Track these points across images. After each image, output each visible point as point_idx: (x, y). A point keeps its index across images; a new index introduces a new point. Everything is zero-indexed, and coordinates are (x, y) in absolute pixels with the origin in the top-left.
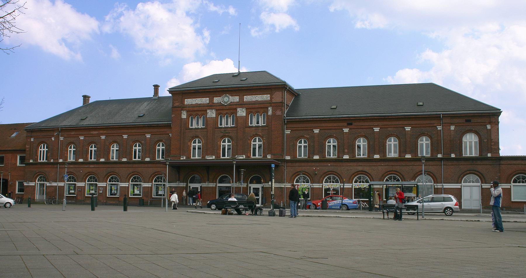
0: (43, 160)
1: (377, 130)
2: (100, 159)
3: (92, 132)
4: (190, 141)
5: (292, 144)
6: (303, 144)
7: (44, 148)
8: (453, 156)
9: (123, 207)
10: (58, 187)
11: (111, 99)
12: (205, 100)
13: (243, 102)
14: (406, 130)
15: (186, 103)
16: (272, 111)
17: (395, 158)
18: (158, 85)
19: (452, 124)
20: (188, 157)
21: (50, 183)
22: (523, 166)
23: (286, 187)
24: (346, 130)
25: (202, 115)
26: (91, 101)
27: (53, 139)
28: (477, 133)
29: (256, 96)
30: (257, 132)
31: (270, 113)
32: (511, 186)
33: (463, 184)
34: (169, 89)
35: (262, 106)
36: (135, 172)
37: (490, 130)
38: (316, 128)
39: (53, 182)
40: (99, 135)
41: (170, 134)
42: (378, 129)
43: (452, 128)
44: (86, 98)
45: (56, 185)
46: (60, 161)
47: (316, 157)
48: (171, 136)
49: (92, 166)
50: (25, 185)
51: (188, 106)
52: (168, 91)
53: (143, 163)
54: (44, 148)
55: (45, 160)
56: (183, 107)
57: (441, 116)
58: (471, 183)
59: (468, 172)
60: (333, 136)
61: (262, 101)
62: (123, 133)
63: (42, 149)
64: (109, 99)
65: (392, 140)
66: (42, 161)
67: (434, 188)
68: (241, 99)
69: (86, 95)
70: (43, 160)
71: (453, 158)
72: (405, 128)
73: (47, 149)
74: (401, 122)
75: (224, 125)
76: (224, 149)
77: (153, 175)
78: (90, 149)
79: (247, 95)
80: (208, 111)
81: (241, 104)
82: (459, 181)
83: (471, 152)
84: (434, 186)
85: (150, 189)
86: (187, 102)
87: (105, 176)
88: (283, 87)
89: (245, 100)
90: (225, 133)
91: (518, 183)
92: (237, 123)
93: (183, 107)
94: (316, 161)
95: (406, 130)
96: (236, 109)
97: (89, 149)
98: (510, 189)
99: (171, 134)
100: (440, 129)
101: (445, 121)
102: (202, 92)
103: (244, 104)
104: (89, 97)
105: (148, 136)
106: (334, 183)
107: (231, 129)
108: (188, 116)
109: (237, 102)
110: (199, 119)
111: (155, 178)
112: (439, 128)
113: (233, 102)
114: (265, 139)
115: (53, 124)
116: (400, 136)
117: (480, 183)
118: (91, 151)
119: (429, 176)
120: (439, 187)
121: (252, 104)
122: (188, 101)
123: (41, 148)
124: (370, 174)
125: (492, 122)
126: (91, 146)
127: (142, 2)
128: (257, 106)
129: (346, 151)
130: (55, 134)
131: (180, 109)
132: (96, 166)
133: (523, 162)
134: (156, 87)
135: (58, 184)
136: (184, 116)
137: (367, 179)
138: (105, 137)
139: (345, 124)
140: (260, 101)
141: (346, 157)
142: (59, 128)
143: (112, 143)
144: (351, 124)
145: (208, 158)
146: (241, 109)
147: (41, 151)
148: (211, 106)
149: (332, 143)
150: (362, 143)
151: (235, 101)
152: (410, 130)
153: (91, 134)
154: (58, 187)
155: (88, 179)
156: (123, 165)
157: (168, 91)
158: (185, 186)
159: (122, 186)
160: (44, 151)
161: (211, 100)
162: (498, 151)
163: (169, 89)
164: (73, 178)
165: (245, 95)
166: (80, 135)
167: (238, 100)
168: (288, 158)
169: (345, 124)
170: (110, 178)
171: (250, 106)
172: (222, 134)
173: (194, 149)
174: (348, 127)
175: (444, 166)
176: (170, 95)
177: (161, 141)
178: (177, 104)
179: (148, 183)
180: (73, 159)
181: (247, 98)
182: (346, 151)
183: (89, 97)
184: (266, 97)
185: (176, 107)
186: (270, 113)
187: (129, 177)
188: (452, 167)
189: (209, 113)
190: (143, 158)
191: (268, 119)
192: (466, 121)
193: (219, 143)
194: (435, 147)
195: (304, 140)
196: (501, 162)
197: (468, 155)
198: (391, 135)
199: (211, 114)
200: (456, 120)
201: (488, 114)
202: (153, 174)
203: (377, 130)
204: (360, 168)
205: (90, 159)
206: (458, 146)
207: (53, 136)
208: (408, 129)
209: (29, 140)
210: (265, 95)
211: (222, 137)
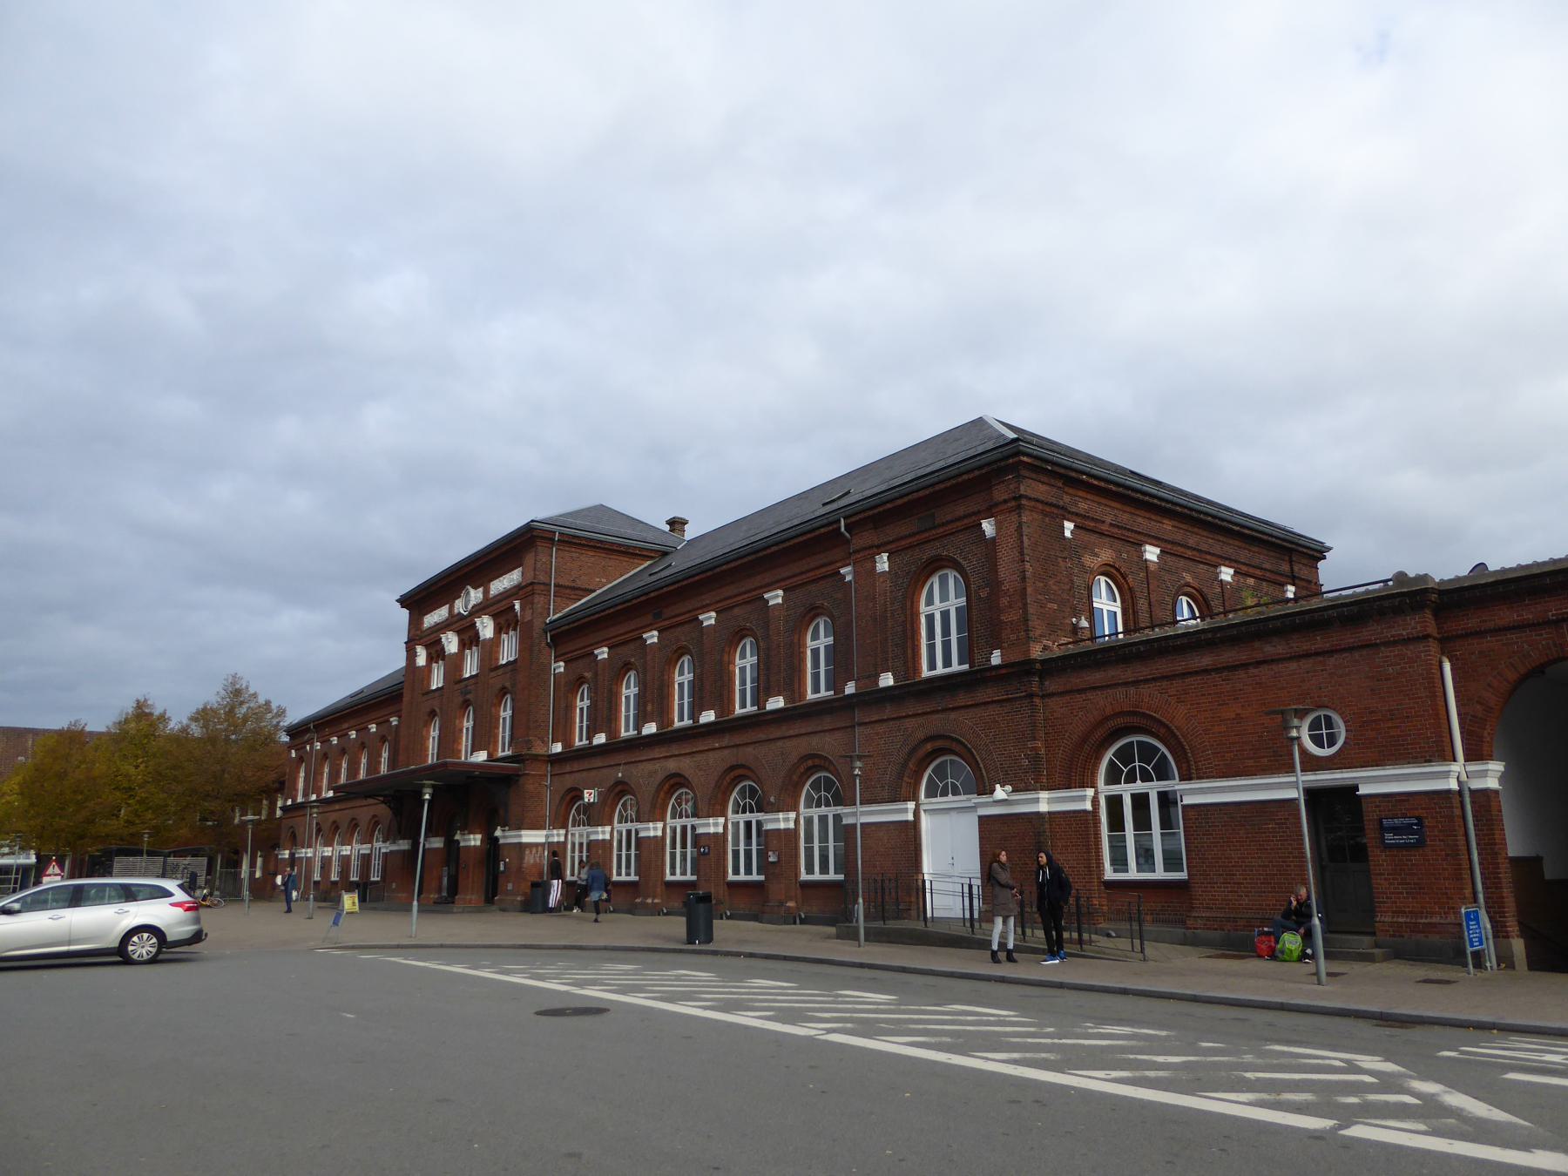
0: (947, 663)
7: (944, 598)
9: (684, 919)
10: (1468, 800)
17: (1523, 574)
22: (1132, 690)
23: (862, 824)
37: (993, 539)
48: (848, 578)
53: (762, 720)
54: (944, 598)
55: (956, 667)
58: (950, 797)
62: (641, 628)
63: (937, 607)
66: (940, 670)
70: (947, 663)
82: (902, 791)
97: (918, 614)
98: (915, 825)
106: (753, 812)
111: (819, 775)
123: (930, 602)
125: (996, 505)
127: (77, 731)
133: (1553, 608)
137: (1164, 756)
147: (930, 618)
154: (1468, 800)
155: (1111, 762)
160: (945, 615)
164: (1147, 752)
166: (596, 646)
170: (822, 774)
180: (960, 663)
188: (881, 728)
196: (1047, 683)
201: (753, 557)
204: (1103, 702)
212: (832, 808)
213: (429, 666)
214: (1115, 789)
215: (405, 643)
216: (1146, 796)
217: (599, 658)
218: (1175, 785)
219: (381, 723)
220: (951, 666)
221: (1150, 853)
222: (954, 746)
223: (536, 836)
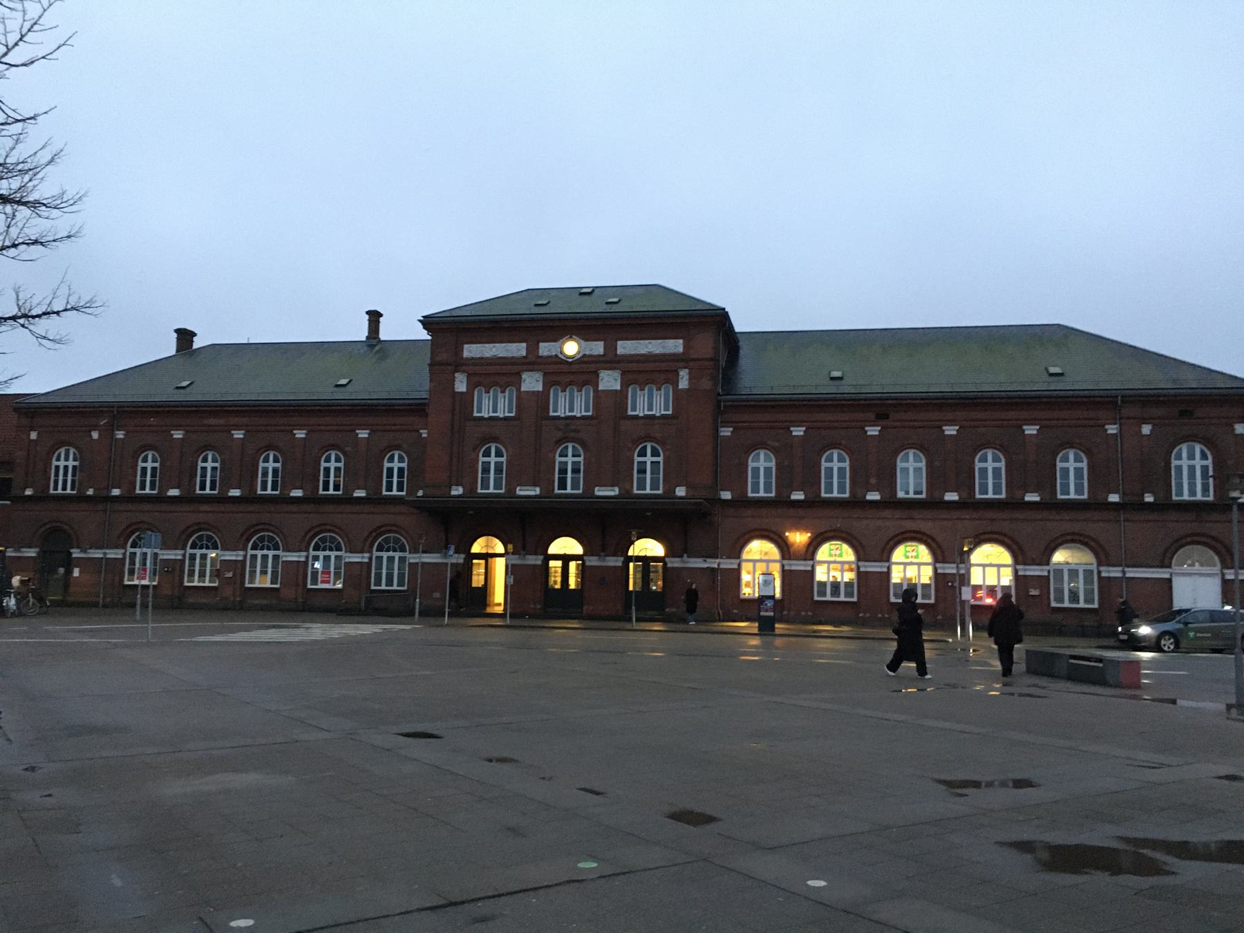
0: (64, 488)
1: (951, 430)
2: (228, 491)
3: (206, 422)
4: (476, 448)
5: (737, 461)
6: (836, 465)
8: (1149, 498)
11: (250, 342)
12: (517, 349)
13: (616, 355)
14: (1027, 432)
15: (466, 354)
16: (690, 379)
18: (379, 310)
19: (1145, 421)
20: (471, 490)
21: (522, 556)
24: (873, 431)
25: (507, 384)
26: (198, 343)
27: (95, 435)
28: (1207, 442)
29: (647, 341)
30: (650, 428)
31: (684, 384)
32: (1049, 572)
33: (1175, 569)
34: (422, 319)
35: (664, 366)
36: (325, 524)
38: (363, 426)
39: (90, 548)
40: (228, 430)
41: (421, 431)
42: (954, 430)
43: (1146, 429)
44: (185, 337)
45: (101, 556)
46: (113, 494)
47: (798, 496)
49: (205, 508)
50: (74, 556)
51: (473, 361)
52: (420, 321)
54: (67, 459)
56: (460, 364)
57: (1117, 401)
59: (1189, 539)
60: (984, 445)
61: (664, 355)
62: (357, 425)
64: (246, 342)
65: (911, 458)
66: (60, 491)
67: (1099, 577)
68: (533, 349)
69: (185, 329)
70: (64, 488)
71: (1149, 503)
72: (792, 429)
73: (76, 463)
74: (1011, 414)
75: (644, 412)
76: (563, 471)
77: (374, 534)
78: (200, 464)
79: (495, 343)
80: (524, 376)
81: (611, 361)
82: (1165, 563)
83: (1192, 492)
84: (1099, 573)
85: (239, 565)
86: (624, 348)
87: (242, 535)
88: (718, 319)
89: (619, 352)
90: (569, 429)
91: (322, 551)
92: (597, 406)
93: (460, 364)
94: (234, 499)
95: (1027, 432)
96: (519, 374)
99: (426, 431)
100: (1115, 432)
101: (1126, 412)
102: (648, 324)
103: (619, 362)
104: (193, 334)
105: (363, 434)
106: (270, 550)
107: (582, 422)
108: (472, 386)
109: (599, 356)
110: (500, 395)
112: (1112, 429)
113: (590, 356)
114: (669, 447)
115: (88, 397)
116: (1011, 448)
117: (1219, 566)
118: (204, 469)
119: (1209, 550)
120: (1112, 575)
121: (638, 362)
122: (471, 351)
124: (933, 539)
126: (203, 458)
128: (650, 366)
129: (873, 481)
130: (102, 423)
131: (449, 368)
132: (216, 507)
134: (374, 317)
135: (105, 554)
136: (461, 386)
137: (339, 542)
138: (244, 434)
139: (872, 416)
140: (657, 355)
141: (873, 496)
142: (1117, 397)
143: (264, 449)
144: (886, 417)
145: (522, 491)
146: (610, 372)
147: (57, 468)
148: (532, 362)
149: (396, 463)
150: (332, 463)
151: (595, 353)
152: (1035, 432)
153: (205, 425)
156: (294, 508)
157: (420, 321)
158: (539, 562)
159: (165, 557)
160: (66, 467)
161: (533, 349)
162: (297, 484)
163: (422, 319)
165: (620, 340)
167: (681, 350)
168: (726, 495)
169: (872, 416)
171: (634, 366)
172: (560, 434)
173: (486, 470)
174: (880, 423)
175: (1126, 523)
176: (423, 335)
177: (398, 447)
178: (444, 356)
179: (362, 552)
181: (626, 347)
182: (873, 481)
183: (193, 334)
184: (675, 346)
185: (441, 364)
186: (684, 384)
187: (308, 537)
189: (527, 382)
190: (163, 489)
191: (676, 399)
192: (1183, 413)
193: (550, 455)
194: (1099, 477)
195: (993, 453)
197: (1186, 497)
198: (986, 445)
199: (610, 381)
200: (1156, 412)
202: (375, 530)
203: (951, 430)
205: (324, 490)
206: (1162, 476)
207: (95, 427)
208: (1031, 430)
209: (24, 437)
210: (672, 341)
211: (559, 442)
212: (398, 553)
213: (470, 392)
214: (254, 552)
215: (429, 365)
216: (394, 557)
217: (297, 436)
218: (407, 554)
219: (1047, 427)
220: (266, 490)
221: (1072, 599)
222: (267, 527)
223: (1164, 573)
